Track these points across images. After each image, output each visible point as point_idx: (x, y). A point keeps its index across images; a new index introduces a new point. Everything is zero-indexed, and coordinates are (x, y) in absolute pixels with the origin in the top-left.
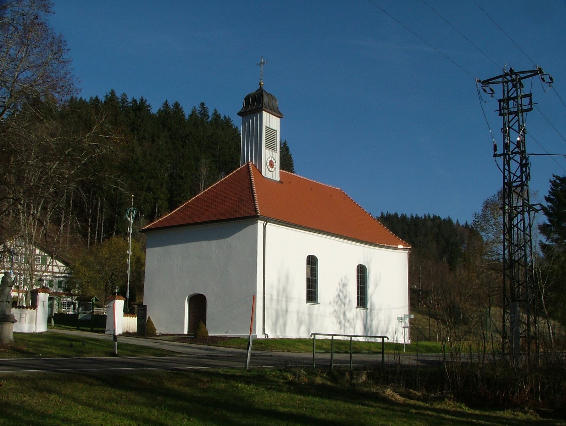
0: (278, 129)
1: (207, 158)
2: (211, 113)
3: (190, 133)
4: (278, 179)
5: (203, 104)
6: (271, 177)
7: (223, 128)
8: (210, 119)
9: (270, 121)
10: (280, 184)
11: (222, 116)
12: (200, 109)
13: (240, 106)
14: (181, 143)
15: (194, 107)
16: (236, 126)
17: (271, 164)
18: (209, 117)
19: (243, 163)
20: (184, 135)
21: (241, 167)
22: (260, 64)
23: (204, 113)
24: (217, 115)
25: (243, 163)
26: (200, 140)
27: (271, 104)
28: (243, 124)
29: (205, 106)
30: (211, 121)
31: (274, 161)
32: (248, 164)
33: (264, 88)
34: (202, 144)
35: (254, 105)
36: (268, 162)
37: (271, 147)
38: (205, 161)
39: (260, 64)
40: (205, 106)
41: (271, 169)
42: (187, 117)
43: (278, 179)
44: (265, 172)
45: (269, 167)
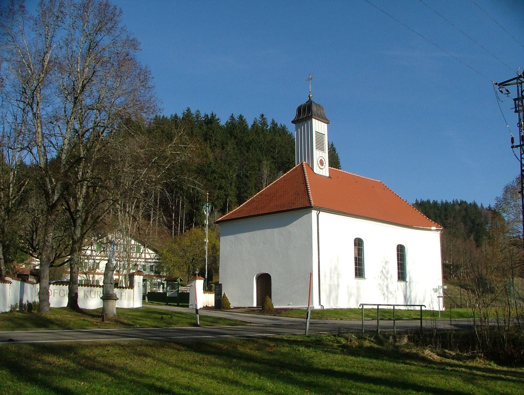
2: (269, 123)
4: (328, 175)
5: (262, 116)
7: (280, 135)
8: (269, 127)
11: (279, 125)
12: (261, 120)
14: (246, 149)
16: (290, 132)
17: (322, 163)
18: (268, 126)
19: (298, 163)
20: (248, 141)
23: (264, 124)
24: (274, 125)
25: (298, 163)
27: (319, 112)
28: (297, 130)
33: (312, 99)
35: (305, 114)
36: (319, 161)
39: (309, 80)
41: (321, 167)
42: (250, 127)
44: (317, 170)
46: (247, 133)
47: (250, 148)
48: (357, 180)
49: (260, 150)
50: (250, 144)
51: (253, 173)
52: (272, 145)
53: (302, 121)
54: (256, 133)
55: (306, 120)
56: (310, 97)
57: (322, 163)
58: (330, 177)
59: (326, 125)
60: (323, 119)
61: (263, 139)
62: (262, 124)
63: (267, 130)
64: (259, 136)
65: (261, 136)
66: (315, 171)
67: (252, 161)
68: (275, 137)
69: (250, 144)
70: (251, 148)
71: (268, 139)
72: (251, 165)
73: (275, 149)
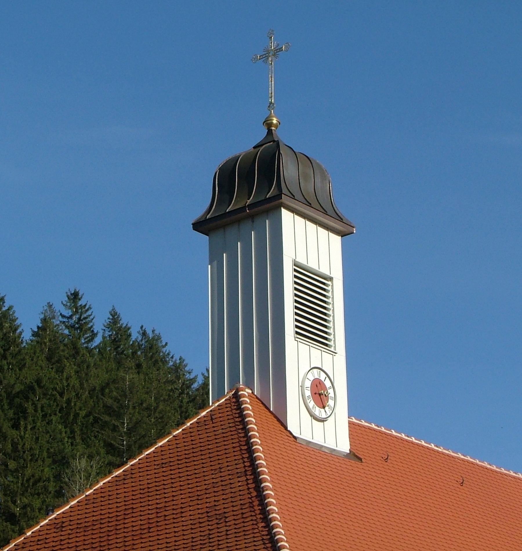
0: (336, 272)
1: (91, 457)
2: (99, 323)
3: (39, 382)
4: (344, 446)
5: (75, 296)
6: (318, 440)
7: (139, 366)
8: (98, 340)
9: (306, 244)
10: (354, 463)
11: (135, 335)
12: (68, 313)
13: (200, 200)
14: (11, 414)
15: (50, 306)
16: (177, 357)
17: (319, 394)
18: (94, 335)
19: (220, 393)
20: (18, 388)
21: (213, 405)
22: (265, 57)
23: (81, 325)
24: (118, 332)
25: (220, 393)
26: (69, 401)
27: (308, 187)
28: (214, 257)
29: (81, 303)
30: (101, 349)
31: (328, 384)
32: (236, 396)
33: (279, 134)
34: (76, 415)
35: (249, 192)
36: (308, 384)
37: (315, 332)
38: (84, 462)
39: (265, 57)
40: (81, 303)
41: (318, 411)
42: (27, 336)
43: (344, 446)
44: (299, 421)
45: (311, 404)
46: (14, 356)
47: (24, 411)
48: (466, 476)
49: (65, 424)
50: (27, 398)
51: (37, 503)
52: (109, 402)
53: (238, 221)
54: (49, 359)
55: (252, 217)
56: (268, 124)
57: (319, 394)
58: (353, 455)
59: (336, 240)
60: (324, 213)
61: (74, 381)
62: (71, 327)
63: (90, 351)
64: (60, 371)
65: (70, 368)
66: (292, 426)
67: (34, 459)
68: (121, 374)
69: (27, 398)
70: (30, 410)
71: (95, 383)
72: (29, 472)
73: (119, 416)
